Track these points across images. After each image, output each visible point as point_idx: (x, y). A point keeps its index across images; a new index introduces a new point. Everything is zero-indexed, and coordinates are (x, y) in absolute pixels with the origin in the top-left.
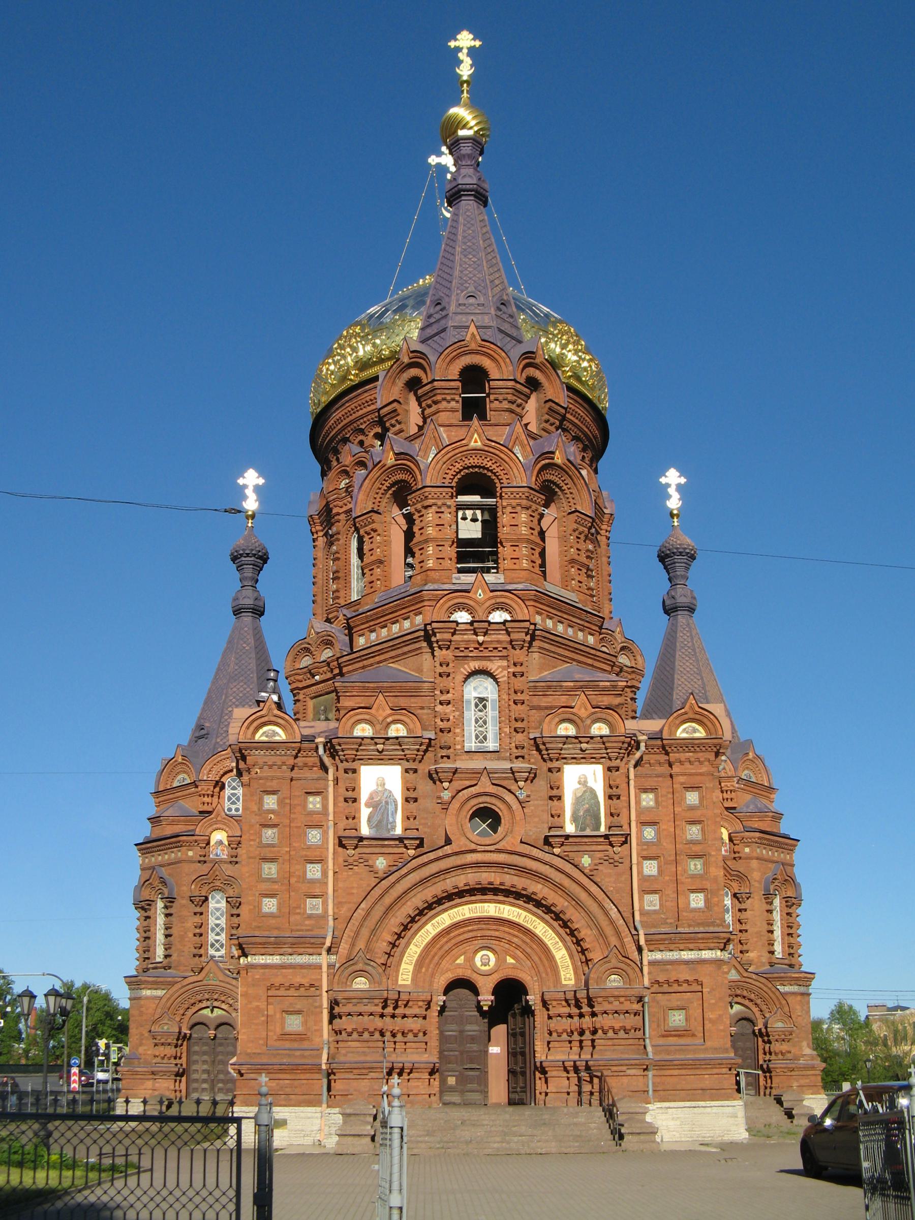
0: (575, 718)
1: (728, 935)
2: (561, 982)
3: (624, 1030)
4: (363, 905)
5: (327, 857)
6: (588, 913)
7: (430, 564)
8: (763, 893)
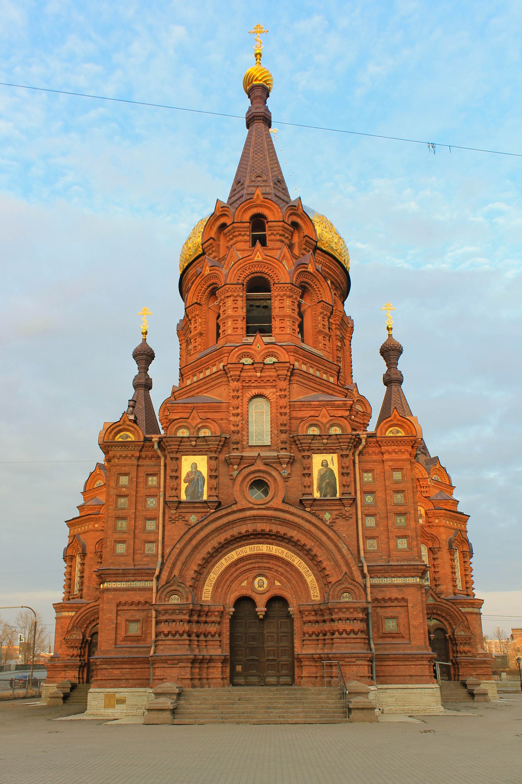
0: (319, 424)
1: (424, 567)
3: (353, 632)
4: (178, 546)
5: (159, 516)
6: (328, 550)
7: (229, 332)
8: (448, 548)
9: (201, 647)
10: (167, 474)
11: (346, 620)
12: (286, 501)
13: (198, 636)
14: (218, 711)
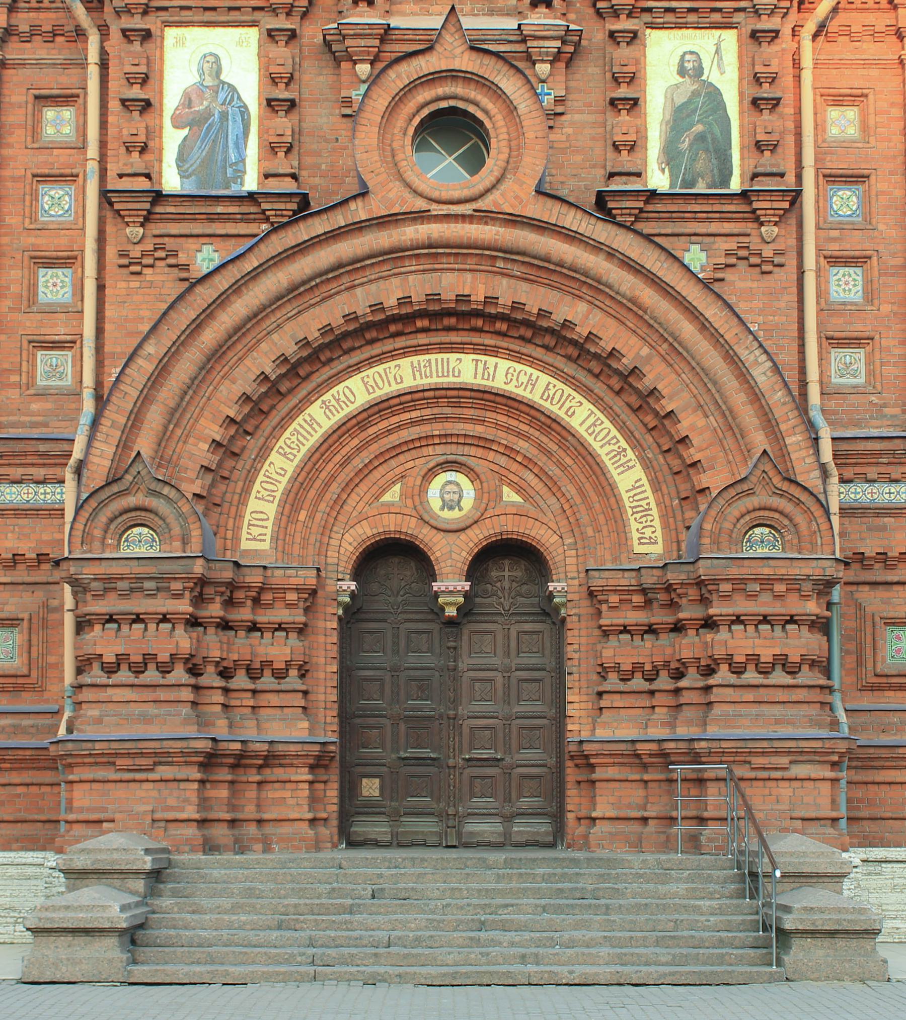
2: (630, 550)
3: (783, 665)
4: (150, 348)
6: (701, 373)
9: (237, 714)
10: (111, 95)
11: (760, 622)
12: (547, 188)
13: (225, 674)
14: (297, 934)
